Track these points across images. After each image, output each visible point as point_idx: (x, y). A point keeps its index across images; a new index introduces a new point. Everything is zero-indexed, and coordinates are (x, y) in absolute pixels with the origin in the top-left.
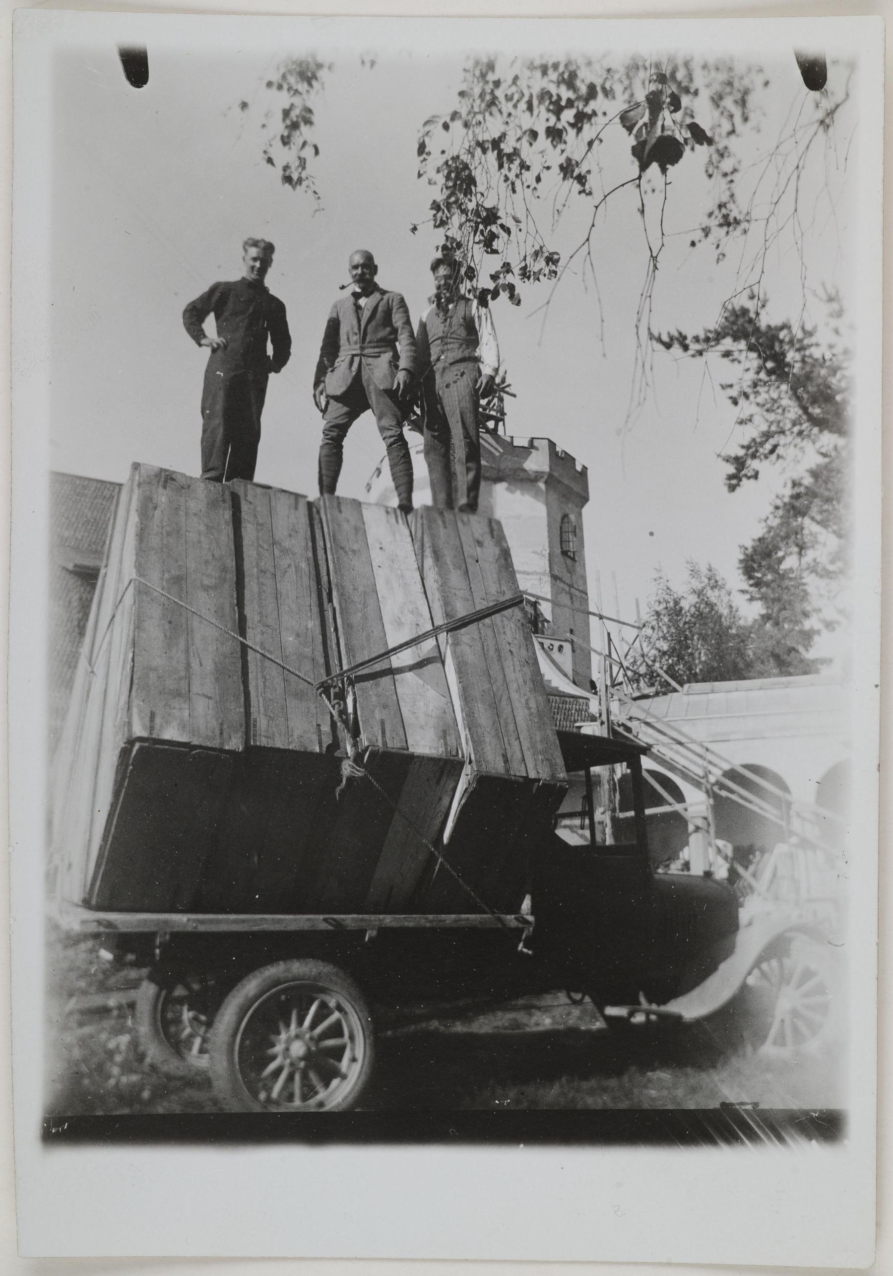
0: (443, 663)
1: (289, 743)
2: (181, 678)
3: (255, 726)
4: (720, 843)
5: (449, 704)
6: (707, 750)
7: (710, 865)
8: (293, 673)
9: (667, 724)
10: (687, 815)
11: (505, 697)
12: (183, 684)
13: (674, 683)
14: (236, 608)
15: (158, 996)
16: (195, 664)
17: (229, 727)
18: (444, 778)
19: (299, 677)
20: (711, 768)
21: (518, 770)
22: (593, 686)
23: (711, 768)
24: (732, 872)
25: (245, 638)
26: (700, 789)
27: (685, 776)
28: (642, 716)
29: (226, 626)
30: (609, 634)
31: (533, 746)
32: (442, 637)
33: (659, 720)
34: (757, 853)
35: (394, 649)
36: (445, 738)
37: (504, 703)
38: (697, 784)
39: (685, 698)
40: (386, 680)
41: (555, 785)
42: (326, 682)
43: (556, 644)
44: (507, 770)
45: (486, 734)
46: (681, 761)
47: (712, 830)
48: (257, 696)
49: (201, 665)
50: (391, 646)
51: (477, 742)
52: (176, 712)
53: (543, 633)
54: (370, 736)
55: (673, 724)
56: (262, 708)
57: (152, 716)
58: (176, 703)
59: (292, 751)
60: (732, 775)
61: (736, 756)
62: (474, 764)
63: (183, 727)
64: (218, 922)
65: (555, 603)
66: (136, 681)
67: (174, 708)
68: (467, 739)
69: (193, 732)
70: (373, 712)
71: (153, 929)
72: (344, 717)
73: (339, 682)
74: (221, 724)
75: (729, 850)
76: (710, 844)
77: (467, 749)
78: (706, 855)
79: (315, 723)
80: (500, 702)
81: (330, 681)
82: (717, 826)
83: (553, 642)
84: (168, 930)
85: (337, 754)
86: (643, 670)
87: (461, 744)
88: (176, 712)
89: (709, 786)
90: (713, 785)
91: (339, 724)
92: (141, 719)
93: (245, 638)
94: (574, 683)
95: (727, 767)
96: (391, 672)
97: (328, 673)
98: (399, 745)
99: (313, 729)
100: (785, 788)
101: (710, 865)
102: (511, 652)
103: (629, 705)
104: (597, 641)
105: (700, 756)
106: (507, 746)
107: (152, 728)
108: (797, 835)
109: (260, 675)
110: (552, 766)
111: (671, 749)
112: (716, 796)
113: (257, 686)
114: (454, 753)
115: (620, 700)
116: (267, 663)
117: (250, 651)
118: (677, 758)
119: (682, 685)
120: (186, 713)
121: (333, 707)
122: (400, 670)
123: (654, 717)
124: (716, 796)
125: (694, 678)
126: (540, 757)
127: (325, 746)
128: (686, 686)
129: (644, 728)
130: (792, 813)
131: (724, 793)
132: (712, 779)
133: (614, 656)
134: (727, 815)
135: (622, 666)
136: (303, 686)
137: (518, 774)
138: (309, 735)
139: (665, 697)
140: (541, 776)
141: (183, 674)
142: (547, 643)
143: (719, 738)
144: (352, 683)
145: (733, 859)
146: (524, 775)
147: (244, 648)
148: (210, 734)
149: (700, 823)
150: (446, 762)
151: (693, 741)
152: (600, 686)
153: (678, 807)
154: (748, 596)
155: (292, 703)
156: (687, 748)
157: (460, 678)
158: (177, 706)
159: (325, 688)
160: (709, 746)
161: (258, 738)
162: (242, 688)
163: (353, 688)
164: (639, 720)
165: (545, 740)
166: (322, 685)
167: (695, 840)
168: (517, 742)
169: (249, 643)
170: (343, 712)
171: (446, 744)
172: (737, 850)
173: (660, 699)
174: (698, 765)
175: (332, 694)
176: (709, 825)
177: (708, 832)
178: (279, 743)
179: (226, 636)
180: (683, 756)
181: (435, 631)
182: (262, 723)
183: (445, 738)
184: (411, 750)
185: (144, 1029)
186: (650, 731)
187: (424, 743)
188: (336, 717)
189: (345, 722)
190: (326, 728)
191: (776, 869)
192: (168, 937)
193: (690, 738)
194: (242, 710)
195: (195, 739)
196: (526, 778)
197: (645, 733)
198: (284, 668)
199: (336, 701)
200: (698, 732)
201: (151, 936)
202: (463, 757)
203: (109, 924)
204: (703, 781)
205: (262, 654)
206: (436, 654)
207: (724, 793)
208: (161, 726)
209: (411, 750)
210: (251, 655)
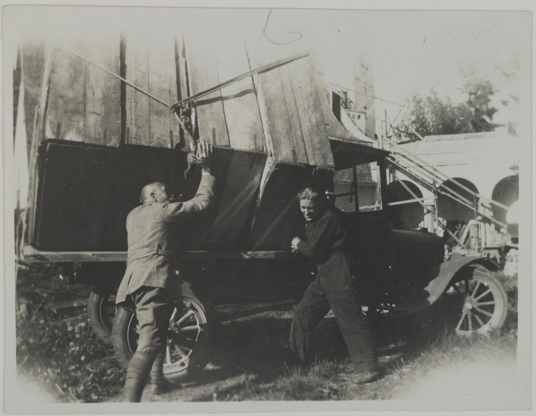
0: (256, 93)
2: (79, 103)
3: (128, 132)
4: (441, 219)
5: (259, 120)
6: (435, 170)
8: (155, 99)
9: (414, 156)
10: (424, 204)
11: (295, 115)
12: (81, 106)
15: (99, 301)
16: (89, 94)
19: (159, 102)
20: (437, 179)
21: (301, 159)
22: (376, 137)
23: (437, 179)
24: (446, 233)
25: (125, 78)
26: (431, 191)
27: (423, 184)
28: (402, 153)
29: (112, 70)
31: (313, 146)
33: (410, 154)
36: (255, 140)
37: (295, 118)
38: (429, 188)
40: (217, 105)
41: (326, 170)
42: (177, 104)
45: (282, 138)
47: (436, 212)
48: (131, 114)
49: (94, 94)
51: (276, 144)
52: (75, 124)
53: (350, 108)
54: (205, 138)
55: (417, 156)
56: (133, 121)
57: (59, 126)
60: (448, 183)
61: (450, 174)
62: (273, 156)
63: (79, 132)
66: (49, 104)
67: (74, 121)
68: (269, 141)
69: (85, 136)
72: (189, 127)
73: (187, 105)
74: (105, 131)
75: (445, 223)
76: (435, 220)
77: (269, 148)
78: (433, 225)
79: (169, 131)
80: (292, 117)
83: (355, 113)
86: (403, 129)
87: (265, 144)
89: (435, 189)
90: (438, 188)
91: (185, 131)
93: (125, 78)
94: (366, 135)
95: (445, 179)
96: (221, 98)
98: (224, 144)
99: (168, 134)
100: (476, 191)
102: (300, 87)
103: (395, 147)
105: (432, 174)
107: (58, 134)
108: (481, 215)
109: (133, 101)
110: (324, 157)
111: (417, 170)
113: (131, 108)
114: (261, 149)
115: (390, 144)
116: (139, 93)
117: (127, 86)
118: (419, 174)
119: (423, 137)
120: (82, 124)
121: (182, 120)
122: (227, 98)
123: (407, 152)
125: (429, 133)
126: (317, 152)
127: (175, 145)
128: (426, 137)
130: (479, 204)
131: (443, 193)
132: (437, 185)
133: (388, 121)
135: (392, 126)
136: (162, 107)
137: (302, 162)
138: (164, 138)
139: (414, 143)
140: (317, 164)
141: (80, 99)
142: (352, 114)
144: (195, 106)
146: (306, 163)
147: (123, 85)
148: (98, 137)
149: (430, 208)
150: (256, 154)
151: (428, 166)
152: (379, 137)
153: (417, 200)
155: (154, 118)
156: (425, 169)
159: (176, 109)
160: (437, 168)
163: (196, 109)
164: (399, 154)
165: (321, 142)
167: (428, 218)
168: (302, 143)
169: (127, 81)
170: (188, 125)
171: (255, 144)
173: (412, 144)
174: (431, 178)
175: (181, 112)
176: (435, 209)
177: (434, 213)
179: (112, 76)
182: (133, 130)
183: (255, 140)
184: (232, 147)
185: (92, 319)
187: (241, 142)
188: (183, 127)
189: (190, 131)
190: (176, 133)
192: (80, 265)
193: (426, 163)
194: (120, 121)
196: (307, 165)
198: (149, 96)
199: (183, 117)
200: (431, 161)
202: (267, 152)
203: (42, 257)
204: (433, 186)
205: (135, 88)
206: (251, 88)
207: (443, 193)
208: (65, 131)
209: (232, 147)
210: (128, 87)
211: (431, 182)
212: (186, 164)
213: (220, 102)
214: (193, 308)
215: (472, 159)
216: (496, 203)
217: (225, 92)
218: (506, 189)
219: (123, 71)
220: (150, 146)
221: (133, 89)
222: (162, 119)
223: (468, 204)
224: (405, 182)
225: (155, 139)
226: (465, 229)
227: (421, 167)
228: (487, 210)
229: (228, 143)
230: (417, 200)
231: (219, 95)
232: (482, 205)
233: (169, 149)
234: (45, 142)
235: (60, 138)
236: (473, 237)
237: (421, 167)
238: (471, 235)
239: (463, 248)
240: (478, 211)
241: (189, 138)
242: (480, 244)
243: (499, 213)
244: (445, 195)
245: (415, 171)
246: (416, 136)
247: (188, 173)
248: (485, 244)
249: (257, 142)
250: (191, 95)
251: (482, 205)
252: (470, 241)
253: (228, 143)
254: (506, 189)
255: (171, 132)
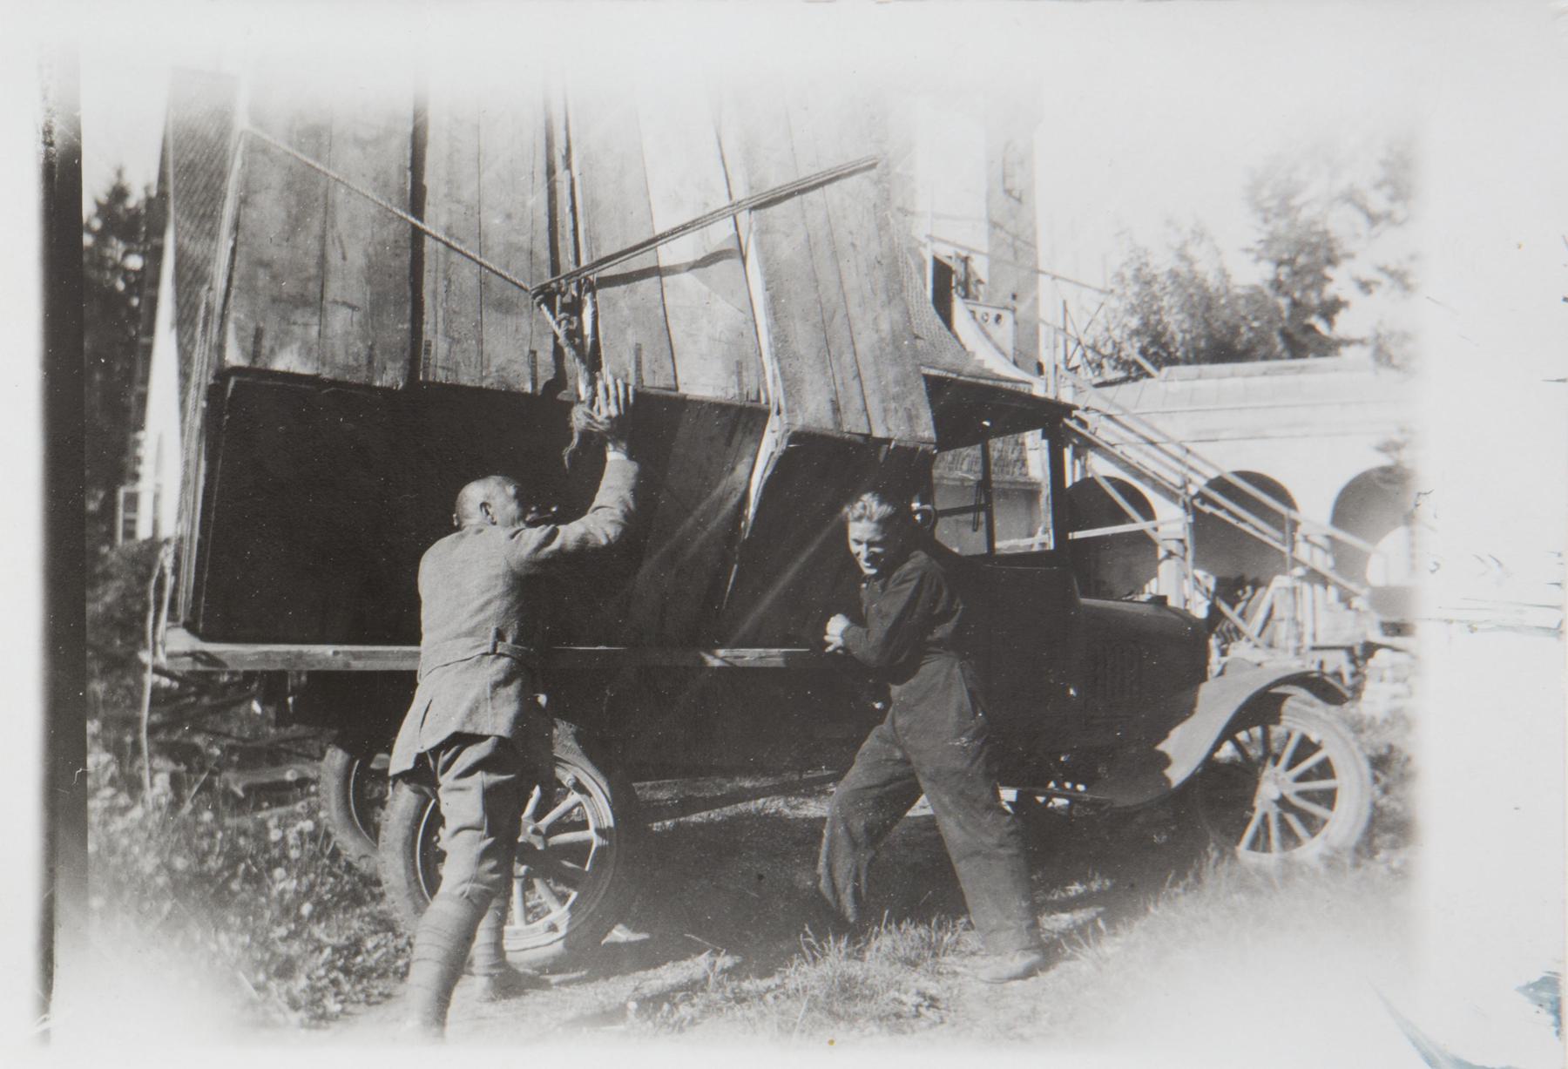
0: (744, 259)
1: (482, 379)
2: (309, 279)
3: (428, 352)
4: (1200, 574)
5: (751, 324)
6: (1188, 451)
7: (1186, 601)
8: (495, 272)
9: (1136, 417)
10: (1155, 536)
12: (313, 287)
13: (1148, 367)
14: (409, 174)
16: (334, 258)
17: (383, 353)
18: (738, 436)
20: (1191, 475)
21: (853, 424)
22: (1040, 369)
23: (1191, 475)
25: (422, 220)
27: (1158, 486)
29: (390, 200)
30: (1065, 303)
32: (744, 217)
33: (1125, 412)
34: (1248, 588)
35: (662, 236)
36: (739, 374)
38: (1171, 495)
39: (1162, 386)
40: (650, 283)
42: (548, 285)
43: (993, 313)
44: (838, 424)
46: (1151, 466)
47: (1190, 555)
49: (344, 258)
50: (658, 231)
51: (791, 385)
52: (297, 330)
53: (976, 298)
56: (441, 326)
57: (258, 335)
58: (299, 316)
59: (487, 390)
60: (1220, 484)
61: (1227, 460)
62: (783, 413)
63: (307, 351)
64: (385, 656)
65: (994, 261)
66: (235, 282)
68: (774, 377)
70: (623, 332)
71: (279, 667)
74: (371, 348)
75: (1211, 583)
76: (1186, 577)
77: (774, 392)
78: (1180, 587)
79: (527, 349)
80: (832, 318)
81: (554, 285)
82: (1197, 552)
84: (306, 668)
85: (563, 396)
87: (765, 383)
88: (297, 330)
91: (566, 350)
92: (241, 340)
93: (422, 220)
94: (1015, 363)
95: (1213, 474)
96: (656, 271)
97: (555, 268)
99: (523, 358)
101: (1186, 601)
102: (853, 245)
103: (1086, 394)
104: (1048, 311)
105: (1178, 460)
106: (840, 389)
107: (255, 355)
108: (1304, 565)
109: (441, 275)
110: (911, 418)
111: (1140, 450)
112: (1197, 513)
114: (753, 397)
116: (455, 257)
117: (428, 242)
120: (314, 331)
121: (559, 324)
122: (672, 270)
123: (1118, 407)
124: (1197, 513)
126: (893, 405)
128: (1165, 370)
129: (1105, 422)
130: (1298, 536)
131: (1207, 509)
132: (1193, 490)
133: (1070, 329)
134: (1209, 534)
137: (854, 430)
141: (313, 271)
142: (980, 311)
143: (1203, 437)
144: (592, 289)
145: (1215, 594)
146: (866, 431)
147: (418, 236)
148: (351, 362)
149: (1174, 546)
150: (741, 410)
151: (1169, 440)
154: (1252, 256)
155: (490, 316)
156: (1162, 450)
157: (767, 283)
158: (300, 321)
159: (547, 296)
160: (1195, 448)
161: (431, 370)
162: (409, 294)
163: (594, 296)
165: (902, 381)
166: (543, 290)
167: (1167, 569)
168: (856, 383)
169: (426, 227)
170: (574, 334)
171: (740, 383)
172: (1220, 582)
173: (1130, 386)
174: (1176, 472)
175: (558, 304)
176: (1186, 549)
177: (1184, 558)
178: (467, 378)
180: (1154, 458)
181: (733, 209)
182: (439, 347)
183: (739, 374)
184: (683, 390)
186: (1112, 426)
187: (703, 381)
188: (562, 340)
189: (579, 350)
190: (545, 356)
191: (1271, 609)
192: (304, 678)
193: (1164, 435)
194: (407, 326)
195: (327, 369)
196: (868, 437)
197: (1106, 430)
198: (481, 265)
200: (1178, 428)
201: (282, 675)
204: (1180, 492)
206: (733, 245)
207: (1207, 509)
210: (429, 243)
211: (1177, 481)
212: (568, 431)
213: (656, 279)
214: (579, 787)
215: (1285, 429)
216: (1340, 535)
217: (667, 254)
218: (1371, 497)
219: (417, 201)
220: (480, 388)
221: (441, 246)
222: (511, 322)
223: (1268, 534)
224: (1108, 479)
225: (493, 369)
226: (1261, 599)
227: (1152, 443)
228: (1318, 554)
229: (672, 382)
230: (1140, 524)
231: (653, 264)
232: (1306, 539)
233: (526, 394)
234: (223, 374)
235: (259, 365)
236: (1282, 620)
237: (1152, 443)
238: (1276, 614)
239: (1256, 646)
240: (1295, 555)
241: (575, 367)
242: (1300, 637)
243: (1348, 562)
244: (1211, 515)
245: (1135, 456)
246: (1140, 368)
247: (574, 452)
248: (1314, 636)
249: (745, 380)
250: (584, 262)
251: (1306, 539)
252: (1275, 628)
253: (672, 382)
254: (1371, 497)
255: (533, 353)
